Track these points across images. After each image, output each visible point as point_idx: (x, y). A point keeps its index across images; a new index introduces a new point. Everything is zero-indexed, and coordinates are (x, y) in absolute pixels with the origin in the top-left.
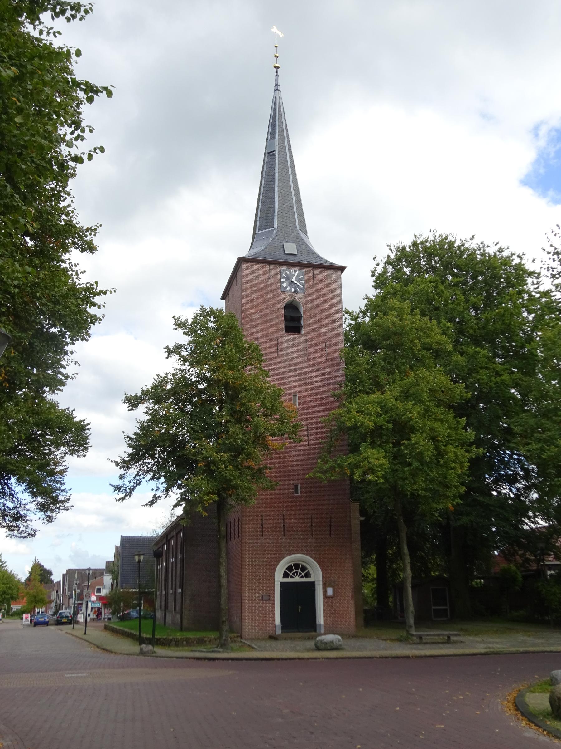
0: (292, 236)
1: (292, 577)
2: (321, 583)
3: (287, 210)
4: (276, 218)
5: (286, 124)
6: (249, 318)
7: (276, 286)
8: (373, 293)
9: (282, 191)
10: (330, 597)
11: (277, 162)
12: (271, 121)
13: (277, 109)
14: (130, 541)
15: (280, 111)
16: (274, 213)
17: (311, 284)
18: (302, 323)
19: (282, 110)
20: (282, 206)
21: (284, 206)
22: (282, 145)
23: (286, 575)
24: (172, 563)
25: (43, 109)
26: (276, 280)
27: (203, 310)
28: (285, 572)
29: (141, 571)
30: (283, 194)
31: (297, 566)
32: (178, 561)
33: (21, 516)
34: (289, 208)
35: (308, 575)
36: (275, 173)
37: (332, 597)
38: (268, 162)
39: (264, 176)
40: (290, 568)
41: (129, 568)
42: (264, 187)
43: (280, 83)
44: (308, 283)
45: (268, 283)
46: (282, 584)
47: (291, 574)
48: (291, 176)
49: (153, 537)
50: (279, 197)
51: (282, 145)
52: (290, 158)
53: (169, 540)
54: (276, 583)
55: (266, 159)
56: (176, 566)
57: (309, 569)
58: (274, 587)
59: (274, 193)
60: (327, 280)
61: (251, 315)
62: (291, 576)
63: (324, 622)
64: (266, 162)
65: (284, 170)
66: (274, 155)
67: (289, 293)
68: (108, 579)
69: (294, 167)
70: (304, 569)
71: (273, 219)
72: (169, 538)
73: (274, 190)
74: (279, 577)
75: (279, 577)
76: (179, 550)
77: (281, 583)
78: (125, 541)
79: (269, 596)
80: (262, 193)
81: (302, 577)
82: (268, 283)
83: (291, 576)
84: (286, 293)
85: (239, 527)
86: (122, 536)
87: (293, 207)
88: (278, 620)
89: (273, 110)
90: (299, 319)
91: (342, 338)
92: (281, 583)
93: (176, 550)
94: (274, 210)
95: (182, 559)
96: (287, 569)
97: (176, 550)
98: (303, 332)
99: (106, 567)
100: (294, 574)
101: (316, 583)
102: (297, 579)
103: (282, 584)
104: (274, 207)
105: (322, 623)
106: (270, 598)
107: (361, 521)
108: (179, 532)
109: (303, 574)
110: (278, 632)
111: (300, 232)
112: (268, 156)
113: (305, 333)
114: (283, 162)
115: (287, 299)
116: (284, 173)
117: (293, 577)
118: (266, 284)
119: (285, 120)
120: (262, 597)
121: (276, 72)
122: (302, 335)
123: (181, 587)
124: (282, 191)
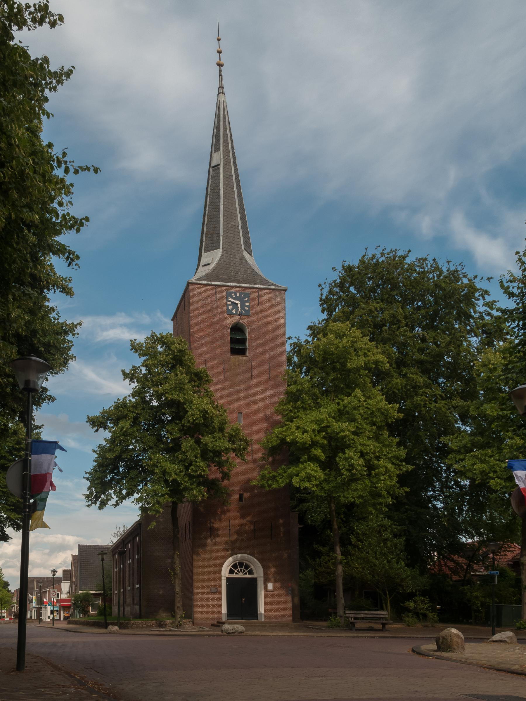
0: (237, 257)
1: (236, 573)
2: (262, 579)
3: (232, 229)
4: (221, 238)
5: (230, 132)
6: (197, 341)
7: (222, 309)
8: (124, 500)
9: (227, 209)
10: (270, 591)
11: (222, 177)
12: (215, 130)
13: (222, 116)
14: (88, 549)
15: (224, 118)
16: (219, 233)
17: (255, 306)
18: (247, 345)
19: (226, 116)
20: (228, 225)
21: (230, 226)
22: (227, 157)
23: (231, 572)
24: (129, 564)
25: (443, 608)
26: (222, 303)
27: (153, 335)
28: (231, 569)
29: (102, 571)
30: (228, 213)
31: (241, 564)
32: (136, 561)
33: (337, 339)
34: (234, 227)
35: (251, 572)
36: (220, 189)
37: (272, 591)
38: (213, 177)
39: (209, 193)
40: (235, 566)
41: (87, 573)
42: (209, 205)
43: (224, 86)
44: (253, 306)
45: (215, 306)
46: (228, 579)
47: (236, 571)
48: (236, 192)
49: (109, 545)
50: (224, 216)
51: (227, 157)
52: (235, 172)
53: (126, 545)
54: (223, 578)
55: (211, 174)
56: (133, 566)
57: (252, 567)
58: (221, 581)
59: (219, 211)
60: (271, 302)
61: (199, 338)
62: (236, 573)
63: (265, 612)
64: (210, 177)
65: (229, 186)
66: (219, 169)
67: (234, 316)
68: (65, 586)
69: (239, 182)
70: (247, 567)
71: (219, 239)
72: (125, 543)
73: (219, 208)
74: (225, 572)
75: (225, 572)
76: (136, 552)
77: (227, 578)
78: (82, 549)
79: (217, 588)
80: (207, 212)
81: (246, 574)
82: (215, 306)
83: (236, 573)
84: (231, 316)
85: (190, 530)
86: (79, 545)
87: (238, 226)
88: (224, 610)
89: (217, 117)
90: (243, 341)
91: (285, 363)
92: (227, 578)
93: (133, 552)
94: (219, 230)
95: (139, 561)
96: (232, 566)
97: (133, 552)
98: (248, 354)
99: (63, 576)
100: (238, 571)
101: (258, 579)
102: (240, 575)
103: (228, 579)
104: (220, 227)
105: (263, 612)
106: (218, 590)
107: (300, 528)
108: (136, 537)
109: (246, 571)
110: (224, 618)
111: (245, 253)
112: (213, 170)
113: (250, 355)
114: (228, 176)
115: (234, 320)
116: (229, 189)
117: (238, 574)
118: (213, 308)
119: (230, 128)
120: (211, 590)
121: (220, 71)
122: (247, 356)
123: (139, 582)
124: (227, 209)
